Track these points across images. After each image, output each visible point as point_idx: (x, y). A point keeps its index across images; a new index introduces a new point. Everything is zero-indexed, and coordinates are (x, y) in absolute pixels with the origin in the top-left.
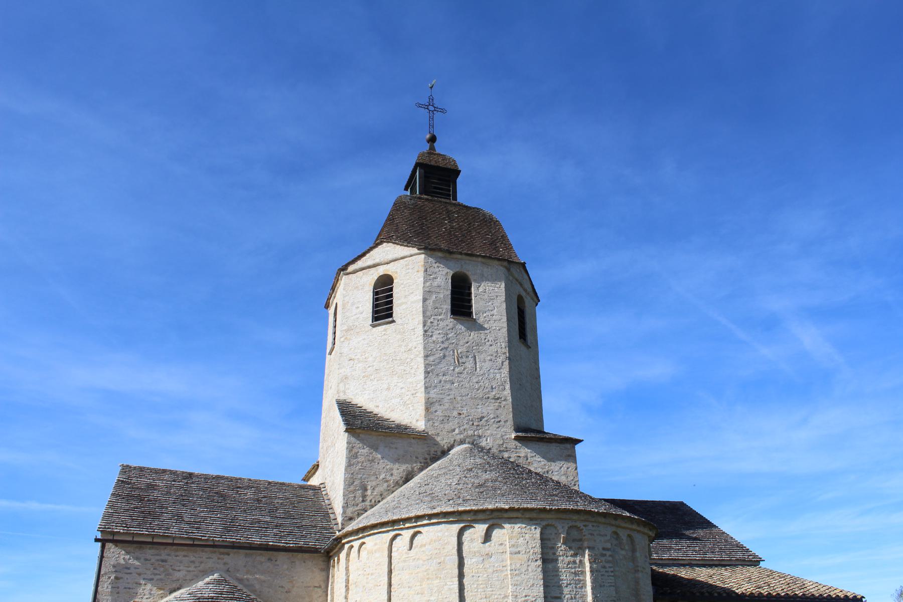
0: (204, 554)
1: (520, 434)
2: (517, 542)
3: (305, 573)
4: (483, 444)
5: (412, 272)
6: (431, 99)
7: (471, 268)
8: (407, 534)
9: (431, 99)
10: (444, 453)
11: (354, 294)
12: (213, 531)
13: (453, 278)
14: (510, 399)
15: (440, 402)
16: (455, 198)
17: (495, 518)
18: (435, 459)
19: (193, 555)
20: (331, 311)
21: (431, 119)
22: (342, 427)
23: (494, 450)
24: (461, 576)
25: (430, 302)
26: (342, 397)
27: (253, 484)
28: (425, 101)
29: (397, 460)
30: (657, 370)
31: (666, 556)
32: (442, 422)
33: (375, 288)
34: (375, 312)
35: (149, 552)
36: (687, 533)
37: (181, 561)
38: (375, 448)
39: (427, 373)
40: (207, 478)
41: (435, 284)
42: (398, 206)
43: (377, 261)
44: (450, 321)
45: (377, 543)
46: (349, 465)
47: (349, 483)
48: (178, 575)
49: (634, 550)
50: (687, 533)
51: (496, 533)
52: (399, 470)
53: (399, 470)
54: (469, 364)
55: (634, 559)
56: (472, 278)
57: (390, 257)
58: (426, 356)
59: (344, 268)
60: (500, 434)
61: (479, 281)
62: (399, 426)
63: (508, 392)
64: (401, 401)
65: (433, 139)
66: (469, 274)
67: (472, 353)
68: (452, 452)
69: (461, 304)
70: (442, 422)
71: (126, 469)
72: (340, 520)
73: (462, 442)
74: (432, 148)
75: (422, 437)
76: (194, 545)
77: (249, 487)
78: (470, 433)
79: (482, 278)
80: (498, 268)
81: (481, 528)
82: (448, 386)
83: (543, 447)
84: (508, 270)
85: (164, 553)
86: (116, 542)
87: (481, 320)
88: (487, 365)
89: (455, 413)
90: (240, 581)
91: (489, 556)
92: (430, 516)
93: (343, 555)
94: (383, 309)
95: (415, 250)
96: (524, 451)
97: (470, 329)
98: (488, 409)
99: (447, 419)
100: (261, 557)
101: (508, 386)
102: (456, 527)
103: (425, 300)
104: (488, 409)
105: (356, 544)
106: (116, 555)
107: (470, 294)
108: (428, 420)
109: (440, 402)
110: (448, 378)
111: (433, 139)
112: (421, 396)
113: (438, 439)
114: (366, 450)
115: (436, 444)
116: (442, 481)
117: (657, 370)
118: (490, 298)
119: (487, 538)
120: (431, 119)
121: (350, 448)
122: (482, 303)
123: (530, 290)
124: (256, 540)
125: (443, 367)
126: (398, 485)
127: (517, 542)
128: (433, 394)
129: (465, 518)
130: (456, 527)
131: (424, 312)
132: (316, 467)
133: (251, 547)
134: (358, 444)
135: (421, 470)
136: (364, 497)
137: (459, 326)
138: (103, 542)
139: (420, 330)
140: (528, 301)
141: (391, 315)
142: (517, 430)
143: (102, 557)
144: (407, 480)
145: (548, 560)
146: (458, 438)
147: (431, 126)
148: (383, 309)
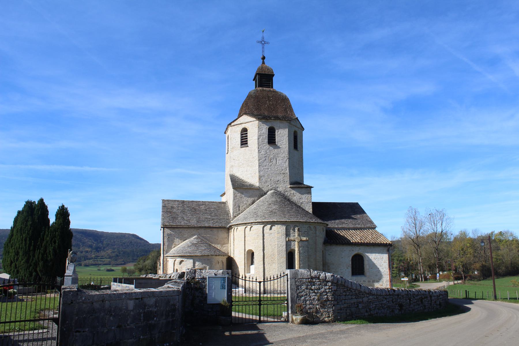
0: (192, 230)
1: (291, 186)
2: (279, 230)
3: (222, 234)
4: (279, 190)
5: (254, 127)
6: (263, 38)
7: (275, 124)
8: (249, 227)
9: (263, 38)
10: (265, 194)
11: (234, 134)
12: (193, 222)
13: (269, 129)
14: (288, 173)
15: (264, 176)
16: (272, 87)
17: (273, 224)
18: (262, 196)
19: (189, 230)
20: (227, 135)
21: (263, 48)
22: (232, 187)
23: (282, 192)
24: (263, 239)
25: (260, 139)
26: (232, 173)
27: (204, 203)
28: (260, 39)
29: (250, 197)
30: (425, 88)
31: (340, 226)
32: (265, 183)
33: (241, 132)
34: (241, 142)
35: (176, 230)
36: (353, 216)
37: (186, 232)
38: (243, 194)
39: (259, 166)
40: (189, 202)
41: (262, 132)
42: (249, 97)
43: (242, 122)
44: (268, 146)
45: (241, 228)
46: (234, 199)
47: (234, 205)
48: (185, 236)
49: (316, 231)
50: (353, 216)
51: (273, 227)
52: (250, 200)
53: (250, 200)
54: (274, 162)
55: (316, 233)
56: (276, 128)
57: (246, 121)
58: (259, 160)
59: (230, 124)
60: (285, 187)
61: (278, 129)
62: (250, 185)
63: (288, 171)
64: (251, 177)
65: (264, 58)
66: (275, 127)
67: (275, 158)
68: (268, 193)
69: (272, 140)
70: (265, 183)
71: (164, 201)
72: (232, 217)
73: (271, 190)
74: (263, 63)
75: (259, 189)
76: (189, 227)
77: (203, 205)
78: (274, 186)
79: (280, 128)
80: (286, 124)
81: (269, 226)
82: (267, 170)
83: (300, 190)
84: (290, 123)
85: (181, 230)
86: (167, 228)
87: (279, 145)
88: (281, 161)
89: (269, 180)
90: (203, 237)
91: (271, 234)
92: (255, 223)
93: (232, 230)
94: (244, 142)
95: (254, 119)
96: (293, 191)
97: (274, 148)
98: (280, 178)
99: (266, 182)
100: (209, 230)
101: (288, 169)
102: (262, 226)
103: (258, 139)
104: (280, 178)
105: (236, 228)
106: (167, 231)
107: (275, 135)
108: (260, 183)
109: (264, 176)
110: (266, 167)
111: (264, 58)
112: (257, 174)
113: (263, 189)
114: (239, 194)
115: (263, 191)
116: (263, 204)
117: (425, 88)
118: (283, 136)
119: (271, 229)
120: (263, 48)
121: (234, 194)
122: (279, 138)
123: (300, 127)
124: (207, 225)
125: (265, 163)
126: (250, 205)
127: (279, 230)
128: (262, 173)
129: (265, 224)
130: (262, 226)
131: (258, 144)
132: (224, 194)
133: (205, 227)
134: (237, 192)
135: (258, 200)
136: (239, 209)
137: (271, 148)
138: (164, 228)
139: (257, 150)
140: (298, 132)
141: (247, 143)
142: (290, 184)
143: (164, 232)
144: (253, 203)
145: (287, 234)
146: (270, 188)
147: (263, 51)
148: (244, 142)
